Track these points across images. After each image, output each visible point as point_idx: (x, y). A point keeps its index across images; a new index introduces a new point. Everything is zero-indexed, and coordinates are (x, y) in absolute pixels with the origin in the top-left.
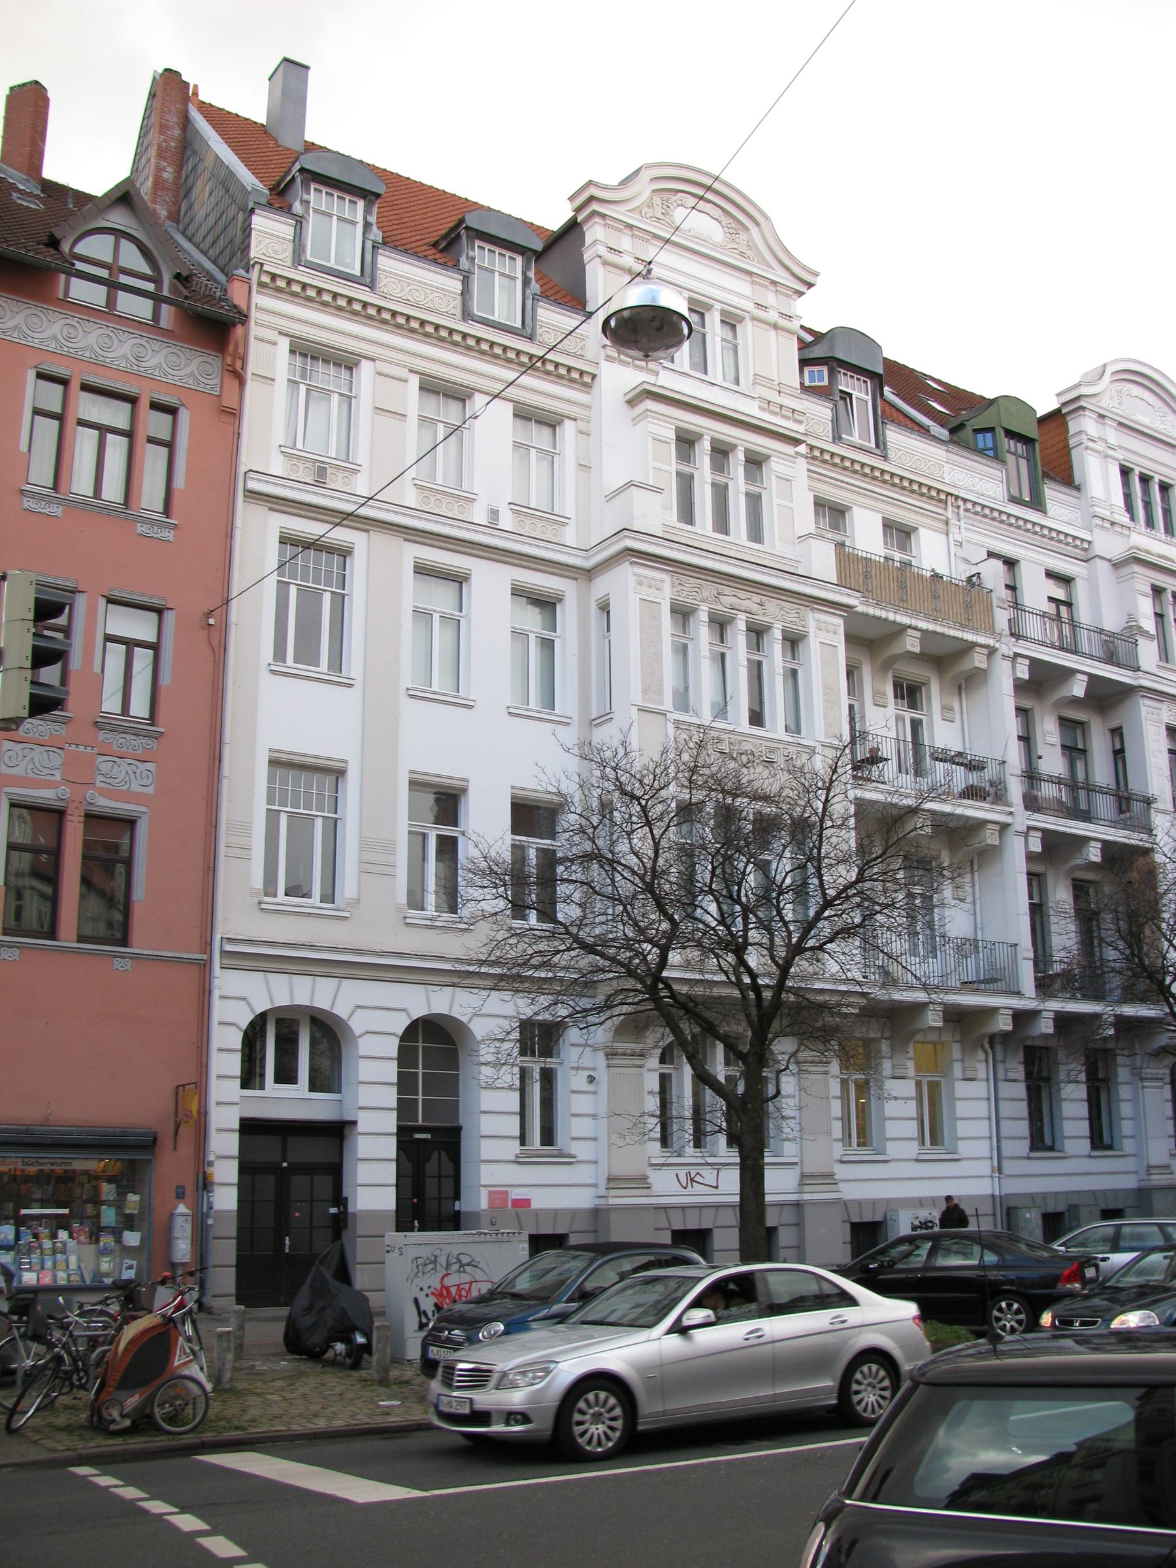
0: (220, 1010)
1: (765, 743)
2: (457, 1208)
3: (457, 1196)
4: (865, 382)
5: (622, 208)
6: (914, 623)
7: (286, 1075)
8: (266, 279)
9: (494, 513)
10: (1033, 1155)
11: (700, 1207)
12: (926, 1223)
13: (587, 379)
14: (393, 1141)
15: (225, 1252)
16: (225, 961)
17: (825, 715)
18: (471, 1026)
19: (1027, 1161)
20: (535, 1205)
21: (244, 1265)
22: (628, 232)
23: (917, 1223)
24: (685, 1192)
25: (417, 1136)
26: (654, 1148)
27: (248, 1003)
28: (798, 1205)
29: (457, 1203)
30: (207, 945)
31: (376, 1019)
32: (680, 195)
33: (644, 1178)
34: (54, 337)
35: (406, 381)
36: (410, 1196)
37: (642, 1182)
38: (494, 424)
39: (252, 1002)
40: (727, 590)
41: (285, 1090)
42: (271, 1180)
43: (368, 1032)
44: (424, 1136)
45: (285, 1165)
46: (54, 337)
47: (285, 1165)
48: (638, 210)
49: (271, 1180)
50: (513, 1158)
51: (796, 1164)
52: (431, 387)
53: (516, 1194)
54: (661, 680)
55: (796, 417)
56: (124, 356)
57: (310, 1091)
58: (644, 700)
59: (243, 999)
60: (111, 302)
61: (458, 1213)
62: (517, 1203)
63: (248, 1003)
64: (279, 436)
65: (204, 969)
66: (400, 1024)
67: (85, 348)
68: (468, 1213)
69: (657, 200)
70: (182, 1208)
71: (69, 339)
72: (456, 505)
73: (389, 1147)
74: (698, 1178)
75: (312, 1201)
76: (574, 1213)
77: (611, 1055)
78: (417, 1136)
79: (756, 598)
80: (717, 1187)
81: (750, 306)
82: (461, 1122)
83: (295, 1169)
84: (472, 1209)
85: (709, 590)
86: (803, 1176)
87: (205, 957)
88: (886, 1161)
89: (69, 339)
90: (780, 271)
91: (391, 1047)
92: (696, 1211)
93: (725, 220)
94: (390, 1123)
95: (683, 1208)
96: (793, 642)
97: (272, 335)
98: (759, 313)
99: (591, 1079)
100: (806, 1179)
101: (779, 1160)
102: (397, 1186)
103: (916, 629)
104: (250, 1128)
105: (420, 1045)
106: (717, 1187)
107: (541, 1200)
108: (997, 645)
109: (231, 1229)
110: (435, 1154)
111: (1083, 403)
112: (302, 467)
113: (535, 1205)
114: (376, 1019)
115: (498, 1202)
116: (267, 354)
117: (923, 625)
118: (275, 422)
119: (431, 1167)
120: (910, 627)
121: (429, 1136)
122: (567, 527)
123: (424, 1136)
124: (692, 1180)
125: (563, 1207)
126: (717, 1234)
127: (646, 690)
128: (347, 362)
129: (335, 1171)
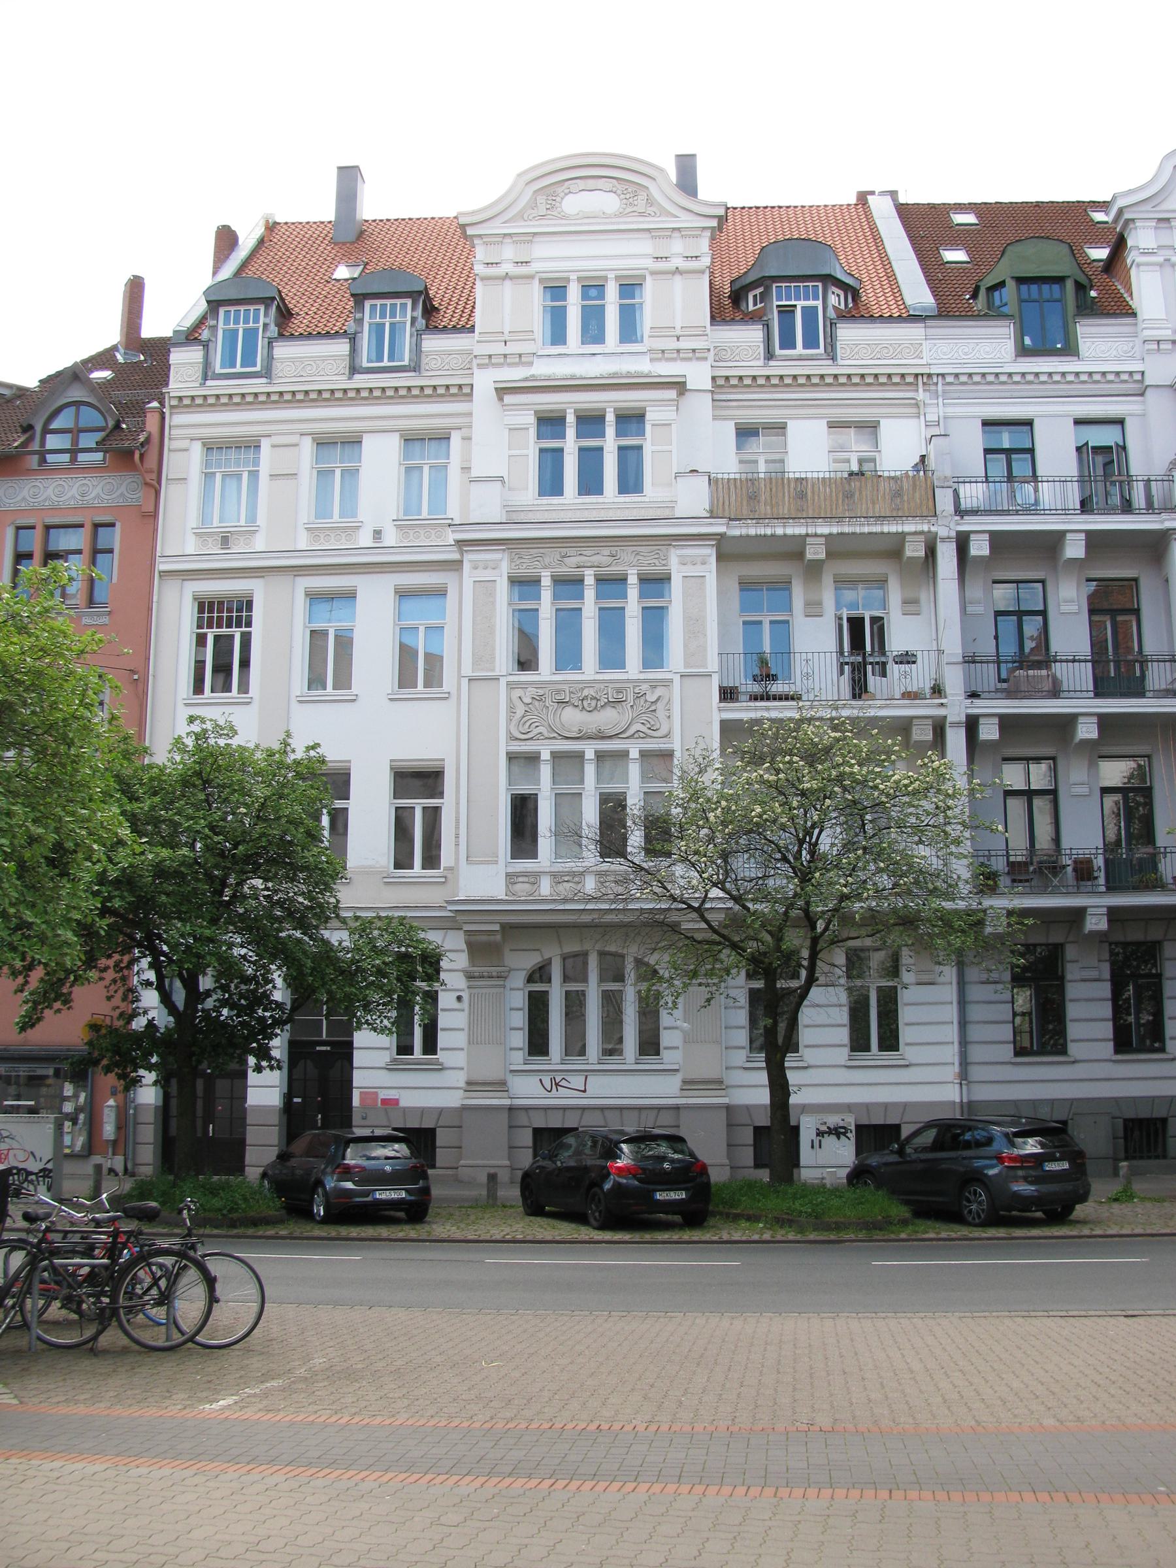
1: (611, 686)
4: (838, 296)
5: (497, 222)
6: (811, 530)
8: (174, 402)
9: (377, 534)
10: (1019, 1060)
11: (564, 1109)
12: (836, 1129)
13: (466, 390)
15: (148, 1134)
17: (685, 646)
19: (844, 1070)
20: (402, 1104)
22: (676, 234)
23: (824, 1128)
24: (549, 1095)
26: (518, 1058)
28: (677, 1108)
32: (567, 183)
33: (503, 1083)
34: (24, 499)
35: (186, 450)
37: (501, 1085)
38: (381, 457)
40: (571, 552)
44: (324, 1048)
46: (24, 499)
48: (520, 216)
51: (677, 1070)
52: (324, 443)
53: (383, 1094)
54: (493, 649)
55: (697, 355)
56: (73, 497)
58: (687, 665)
60: (74, 460)
62: (385, 1102)
64: (193, 521)
67: (45, 500)
69: (541, 199)
70: (111, 1102)
71: (35, 496)
72: (343, 535)
74: (563, 1083)
75: (232, 1098)
76: (441, 1111)
77: (470, 976)
79: (606, 551)
80: (584, 1091)
81: (649, 263)
85: (552, 556)
86: (684, 1082)
88: (806, 1068)
89: (35, 496)
90: (684, 216)
92: (636, 1113)
93: (620, 187)
95: (546, 1109)
96: (654, 583)
97: (184, 444)
98: (662, 265)
99: (459, 998)
100: (689, 1084)
101: (801, 1064)
103: (816, 535)
106: (584, 1091)
107: (408, 1100)
108: (933, 529)
109: (149, 1117)
111: (1127, 216)
112: (210, 540)
113: (402, 1104)
116: (184, 461)
117: (824, 530)
118: (189, 516)
120: (807, 535)
122: (258, 534)
123: (324, 1048)
124: (557, 1085)
125: (914, 1100)
126: (439, 1133)
127: (477, 661)
128: (353, 442)
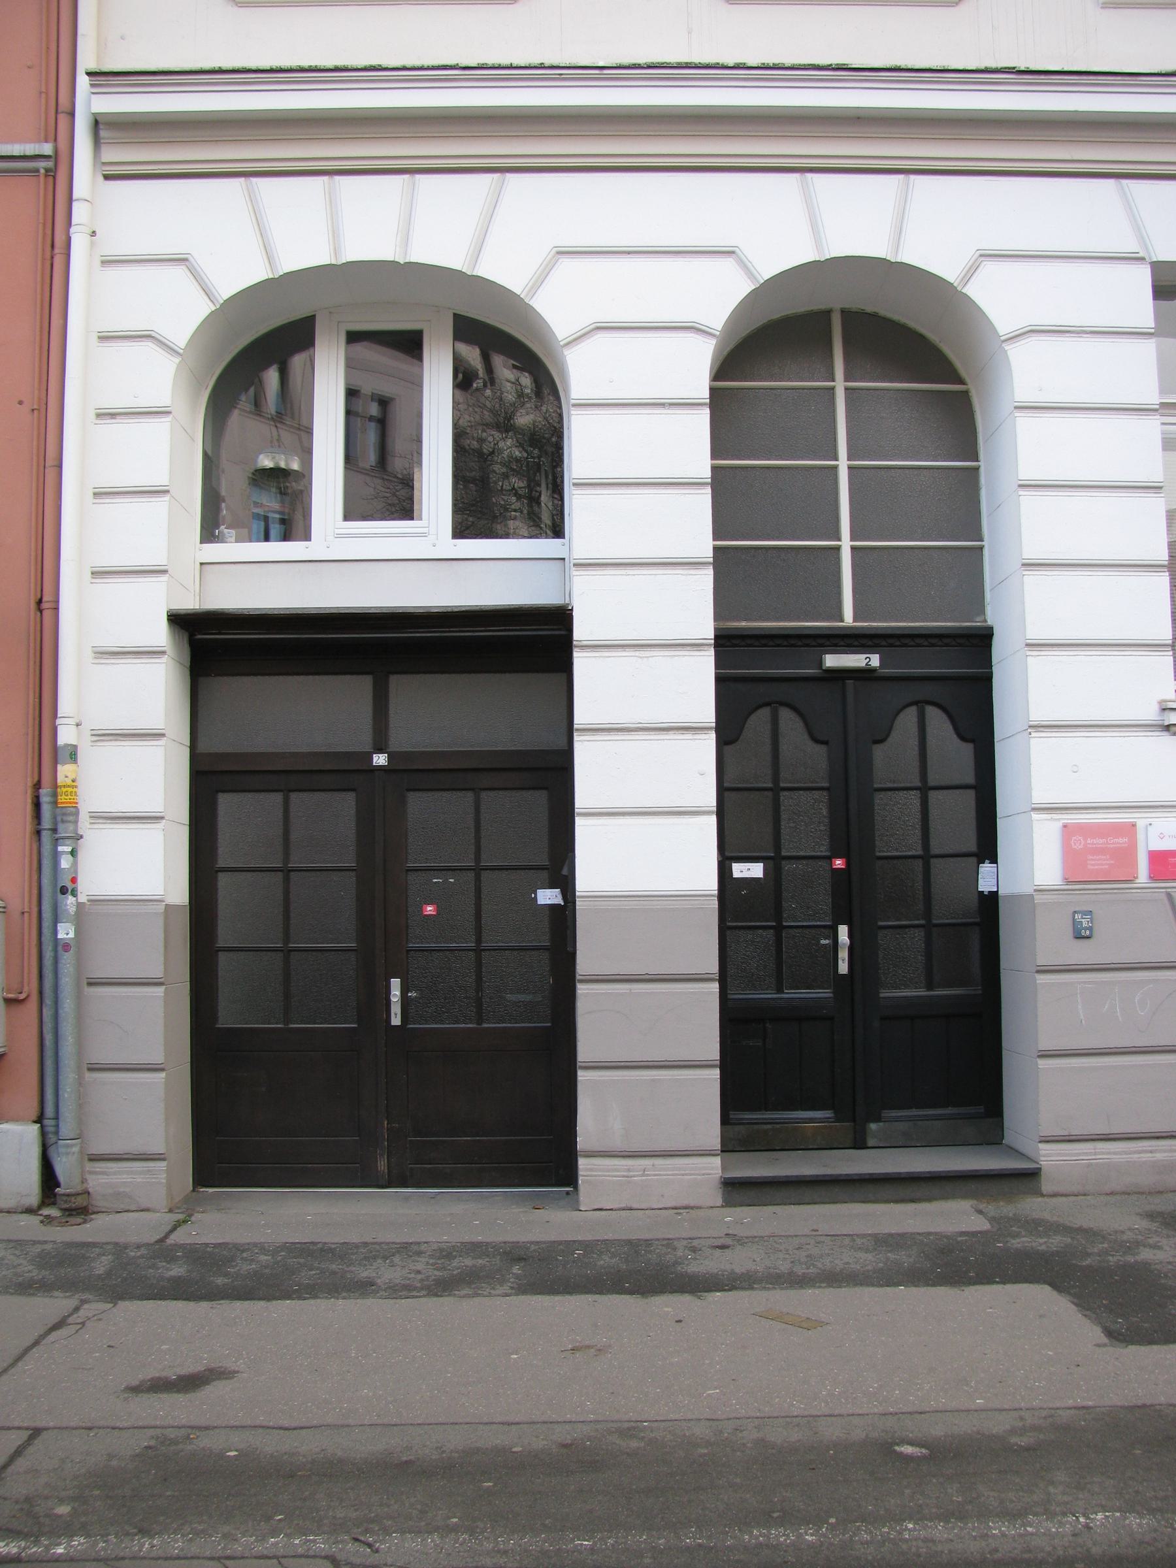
0: (94, 297)
2: (986, 884)
3: (987, 849)
7: (383, 488)
14: (705, 666)
16: (111, 154)
18: (973, 291)
21: (224, 1064)
25: (832, 661)
27: (196, 275)
29: (986, 868)
30: (61, 112)
31: (637, 296)
36: (823, 851)
39: (203, 261)
41: (383, 537)
42: (345, 805)
43: (598, 328)
45: (380, 760)
47: (380, 760)
49: (345, 805)
50: (1150, 713)
57: (461, 531)
59: (181, 260)
61: (991, 901)
63: (196, 275)
65: (53, 173)
66: (716, 299)
68: (1015, 898)
73: (694, 689)
78: (832, 661)
82: (992, 617)
83: (419, 773)
84: (1026, 889)
87: (47, 149)
91: (692, 368)
94: (690, 607)
102: (721, 813)
104: (214, 645)
105: (840, 385)
110: (909, 718)
114: (637, 296)
115: (1098, 864)
119: (893, 757)
121: (875, 661)
129: (546, 776)
